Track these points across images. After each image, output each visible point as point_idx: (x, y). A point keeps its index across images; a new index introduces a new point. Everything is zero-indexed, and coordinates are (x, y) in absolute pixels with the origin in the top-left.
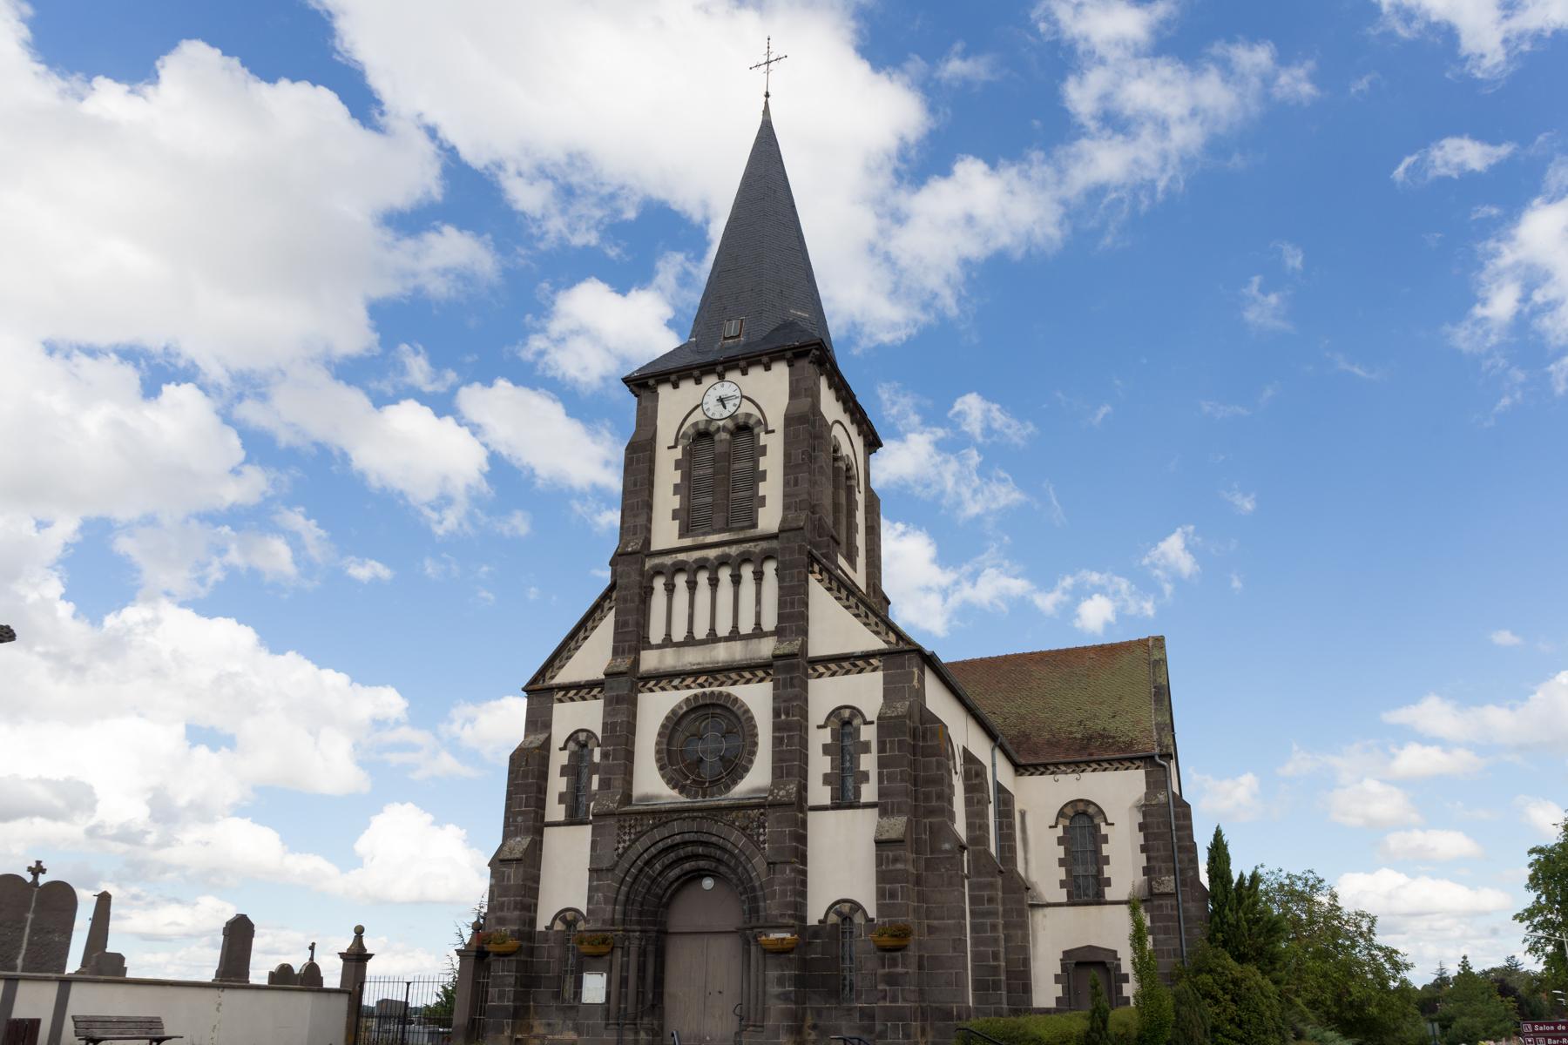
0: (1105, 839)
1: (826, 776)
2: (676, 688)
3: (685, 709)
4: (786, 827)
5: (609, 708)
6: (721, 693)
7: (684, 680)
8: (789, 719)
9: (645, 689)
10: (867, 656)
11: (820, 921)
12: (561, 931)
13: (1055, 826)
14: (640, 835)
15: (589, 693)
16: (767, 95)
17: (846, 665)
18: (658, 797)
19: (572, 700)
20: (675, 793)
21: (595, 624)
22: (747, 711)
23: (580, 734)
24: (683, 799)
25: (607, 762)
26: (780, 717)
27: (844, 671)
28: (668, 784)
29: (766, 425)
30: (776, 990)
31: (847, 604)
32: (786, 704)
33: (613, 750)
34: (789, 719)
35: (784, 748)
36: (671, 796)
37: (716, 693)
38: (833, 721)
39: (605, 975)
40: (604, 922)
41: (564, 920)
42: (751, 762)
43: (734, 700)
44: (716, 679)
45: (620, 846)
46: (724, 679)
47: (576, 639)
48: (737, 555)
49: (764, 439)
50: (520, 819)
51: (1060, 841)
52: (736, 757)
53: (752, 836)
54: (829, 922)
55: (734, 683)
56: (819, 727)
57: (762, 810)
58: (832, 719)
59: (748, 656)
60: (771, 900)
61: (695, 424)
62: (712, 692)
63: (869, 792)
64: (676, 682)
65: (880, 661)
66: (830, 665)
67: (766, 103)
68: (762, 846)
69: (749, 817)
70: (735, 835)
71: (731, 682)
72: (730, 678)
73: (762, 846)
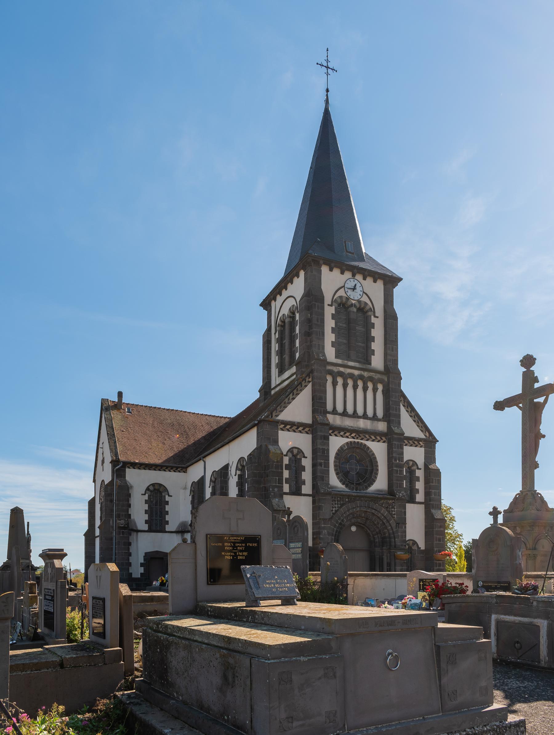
0: (167, 503)
2: (342, 436)
6: (362, 443)
7: (345, 433)
10: (419, 440)
13: (145, 494)
14: (342, 505)
15: (297, 429)
16: (327, 91)
17: (411, 442)
18: (336, 487)
19: (288, 430)
20: (343, 486)
21: (298, 392)
22: (373, 454)
23: (294, 450)
24: (347, 490)
25: (321, 468)
26: (397, 461)
28: (340, 482)
29: (374, 312)
31: (411, 414)
33: (324, 462)
34: (400, 462)
36: (341, 488)
37: (360, 443)
38: (406, 466)
42: (376, 478)
44: (360, 436)
45: (334, 509)
46: (363, 437)
47: (288, 397)
48: (368, 377)
49: (373, 320)
50: (276, 490)
51: (146, 502)
55: (367, 440)
57: (393, 501)
61: (341, 297)
62: (358, 442)
63: (307, 488)
64: (342, 433)
65: (423, 443)
67: (327, 95)
69: (388, 503)
70: (383, 510)
71: (366, 439)
72: (366, 437)
73: (394, 516)
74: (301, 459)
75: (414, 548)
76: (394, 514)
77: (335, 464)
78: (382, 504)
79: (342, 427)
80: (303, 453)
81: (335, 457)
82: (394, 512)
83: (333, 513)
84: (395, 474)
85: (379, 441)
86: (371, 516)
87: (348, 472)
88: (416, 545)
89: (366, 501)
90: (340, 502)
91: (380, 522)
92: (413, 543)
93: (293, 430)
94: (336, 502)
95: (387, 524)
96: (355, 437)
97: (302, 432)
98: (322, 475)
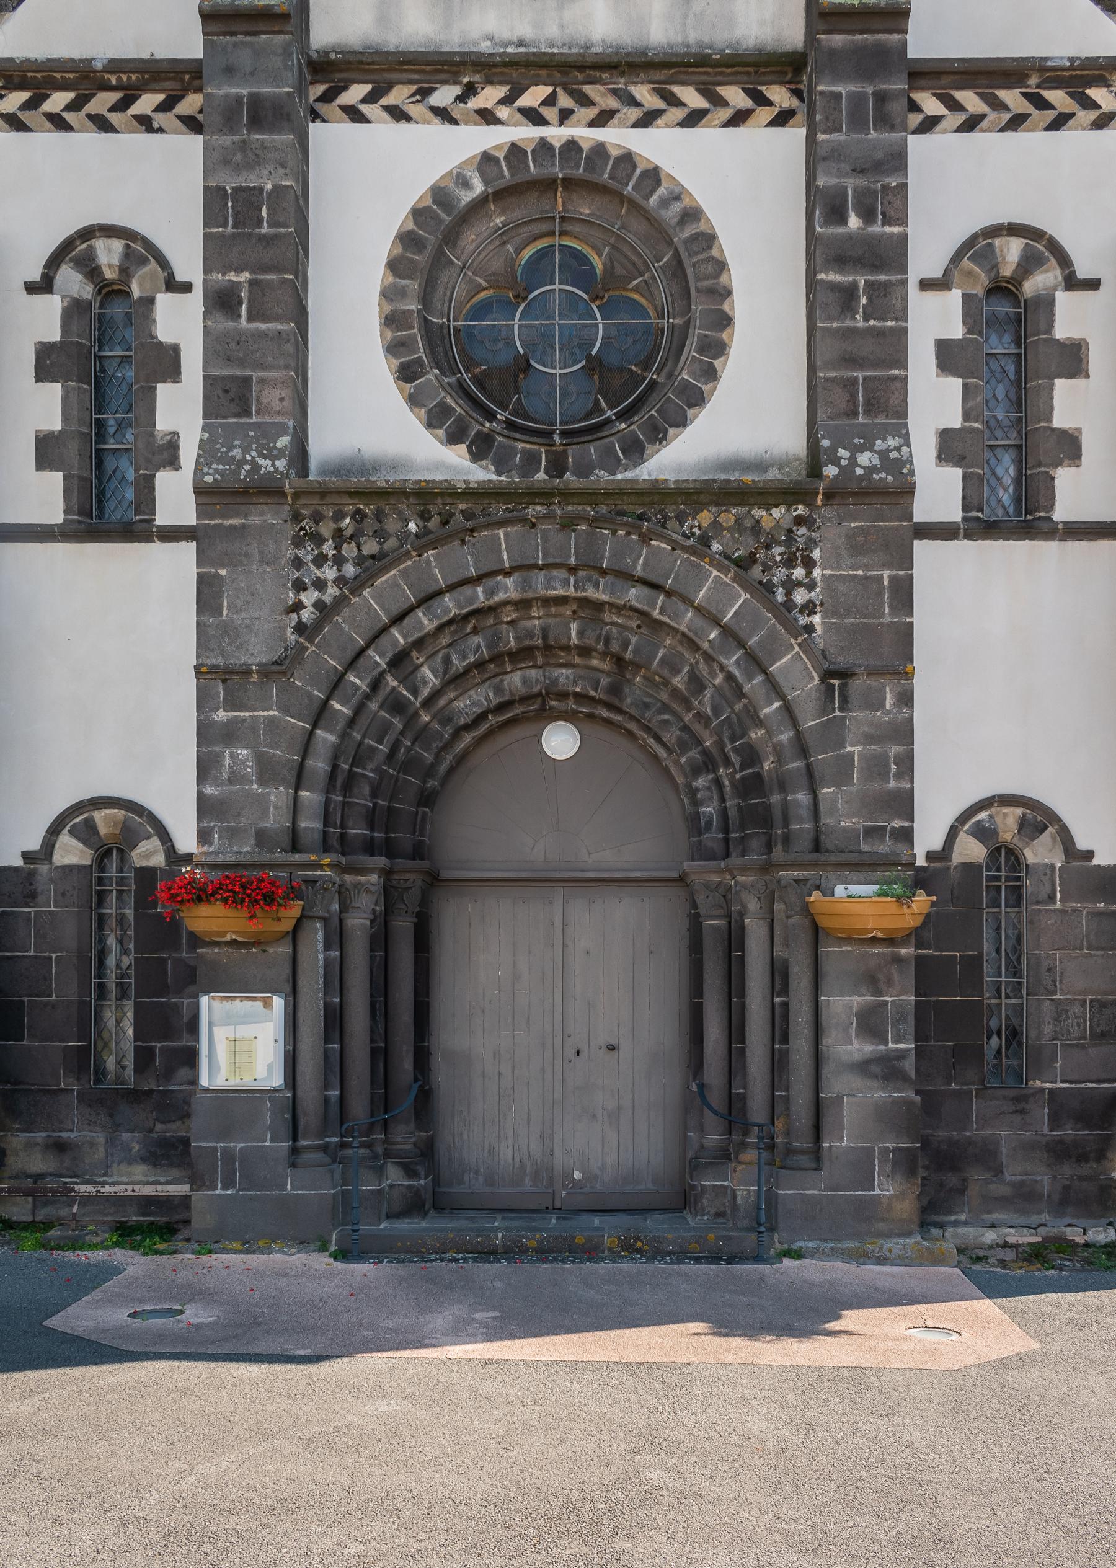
1: (946, 437)
2: (443, 114)
3: (478, 187)
4: (883, 566)
5: (227, 140)
6: (600, 150)
7: (470, 90)
8: (876, 229)
9: (329, 109)
11: (930, 856)
12: (80, 867)
15: (121, 106)
17: (1012, 97)
19: (58, 122)
26: (843, 220)
27: (1006, 117)
28: (430, 425)
30: (860, 1048)
32: (862, 182)
33: (252, 283)
34: (876, 229)
35: (859, 322)
36: (439, 465)
37: (585, 146)
38: (970, 274)
39: (278, 1002)
40: (262, 838)
41: (87, 833)
42: (711, 374)
43: (645, 174)
44: (585, 101)
45: (309, 598)
46: (612, 103)
52: (646, 365)
53: (769, 588)
54: (957, 858)
55: (647, 120)
56: (926, 285)
57: (801, 510)
58: (966, 263)
59: (692, 36)
60: (837, 785)
62: (572, 145)
64: (444, 96)
66: (960, 95)
68: (803, 620)
69: (757, 525)
71: (634, 114)
72: (634, 103)
73: (803, 620)
74: (151, 301)
75: (1035, 855)
76: (810, 601)
77: (388, 308)
78: (705, 541)
79: (446, 49)
80: (163, 263)
81: (393, 265)
82: (811, 587)
83: (300, 628)
84: (831, 319)
85: (739, 118)
86: (634, 639)
87: (523, 366)
88: (1051, 830)
89: (568, 524)
90: (358, 546)
91: (713, 674)
92: (1023, 823)
93: (90, 117)
94: (328, 548)
95: (754, 685)
96: (550, 113)
97: (155, 125)
98: (238, 373)
